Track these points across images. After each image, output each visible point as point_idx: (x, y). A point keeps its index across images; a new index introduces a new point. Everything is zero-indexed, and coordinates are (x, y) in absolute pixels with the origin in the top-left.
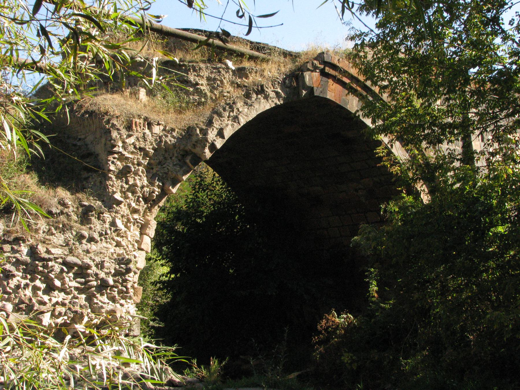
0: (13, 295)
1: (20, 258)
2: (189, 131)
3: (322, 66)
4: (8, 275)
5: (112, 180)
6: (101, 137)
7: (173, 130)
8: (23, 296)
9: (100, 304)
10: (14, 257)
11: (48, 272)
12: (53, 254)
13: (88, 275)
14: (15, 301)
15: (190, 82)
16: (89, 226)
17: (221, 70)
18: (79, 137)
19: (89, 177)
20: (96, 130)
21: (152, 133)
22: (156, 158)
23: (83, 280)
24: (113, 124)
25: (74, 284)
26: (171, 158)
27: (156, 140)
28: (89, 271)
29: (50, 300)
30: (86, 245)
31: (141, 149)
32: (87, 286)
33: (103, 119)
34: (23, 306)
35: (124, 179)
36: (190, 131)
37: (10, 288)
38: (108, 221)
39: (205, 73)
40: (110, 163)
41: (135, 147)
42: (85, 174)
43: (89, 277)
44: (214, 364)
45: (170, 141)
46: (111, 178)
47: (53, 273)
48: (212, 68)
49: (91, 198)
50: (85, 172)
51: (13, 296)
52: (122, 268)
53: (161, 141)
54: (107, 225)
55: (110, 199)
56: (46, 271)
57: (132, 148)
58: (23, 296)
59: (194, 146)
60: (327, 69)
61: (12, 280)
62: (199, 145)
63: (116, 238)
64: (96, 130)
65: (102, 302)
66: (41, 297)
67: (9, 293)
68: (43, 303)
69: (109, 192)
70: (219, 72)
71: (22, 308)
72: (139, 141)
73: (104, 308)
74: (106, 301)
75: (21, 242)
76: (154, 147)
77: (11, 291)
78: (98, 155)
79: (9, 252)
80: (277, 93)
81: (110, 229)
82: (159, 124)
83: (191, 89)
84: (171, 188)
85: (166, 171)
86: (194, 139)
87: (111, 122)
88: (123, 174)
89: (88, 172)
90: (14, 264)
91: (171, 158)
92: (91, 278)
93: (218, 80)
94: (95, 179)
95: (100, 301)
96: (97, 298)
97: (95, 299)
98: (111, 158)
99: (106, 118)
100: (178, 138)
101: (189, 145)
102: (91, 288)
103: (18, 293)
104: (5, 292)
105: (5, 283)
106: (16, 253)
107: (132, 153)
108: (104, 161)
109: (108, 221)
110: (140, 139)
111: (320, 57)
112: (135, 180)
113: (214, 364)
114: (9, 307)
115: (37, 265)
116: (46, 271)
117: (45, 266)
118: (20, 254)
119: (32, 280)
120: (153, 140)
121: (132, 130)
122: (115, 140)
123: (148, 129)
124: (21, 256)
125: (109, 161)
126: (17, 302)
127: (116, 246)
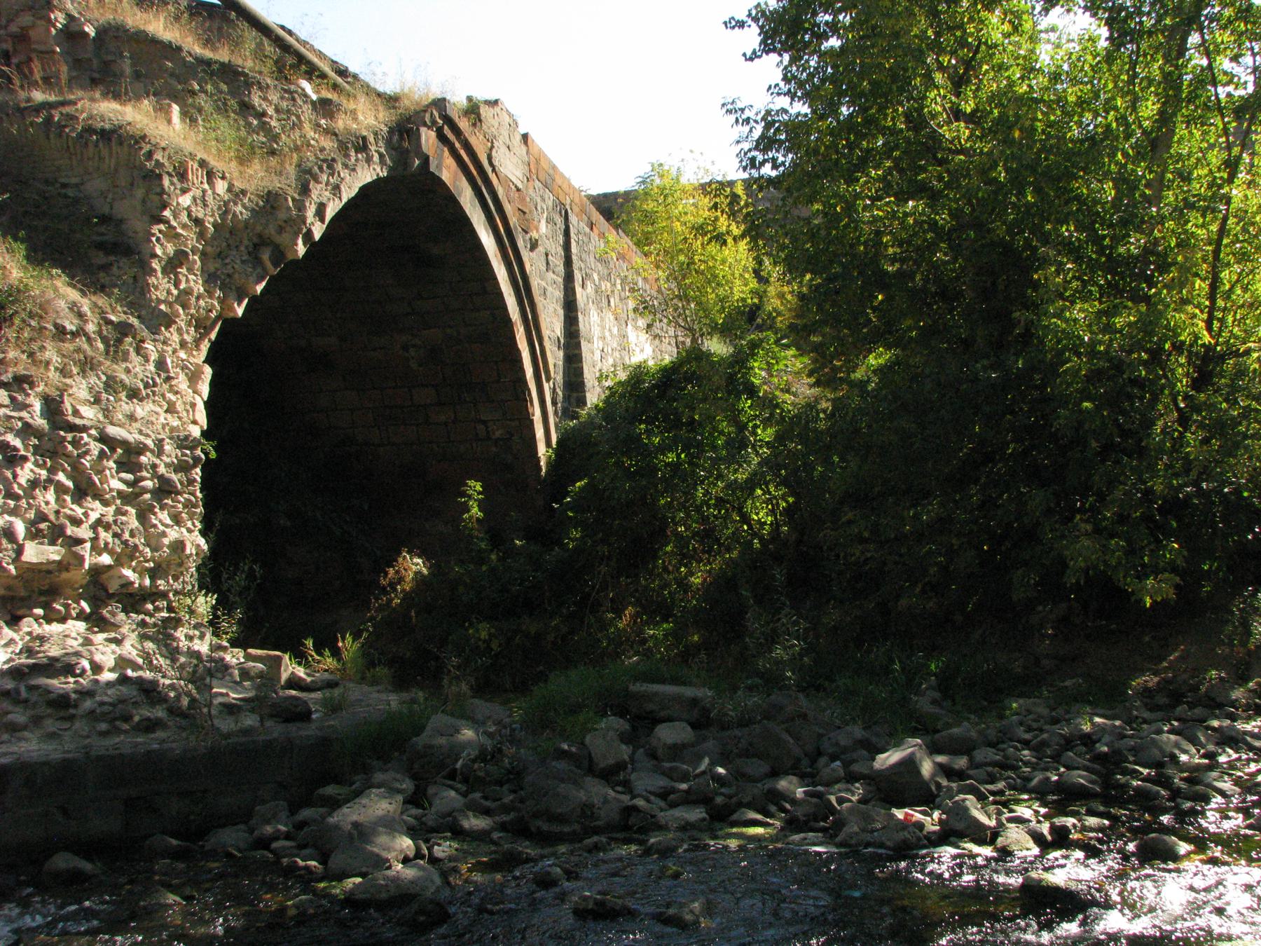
0: (24, 500)
1: (30, 421)
2: (272, 200)
3: (441, 122)
4: (14, 460)
5: (156, 276)
6: (132, 184)
7: (244, 192)
8: (43, 504)
9: (161, 528)
10: (20, 419)
11: (79, 456)
12: (82, 418)
13: (140, 467)
14: (28, 516)
15: (253, 107)
16: (124, 366)
17: (296, 96)
18: (63, 180)
19: (111, 264)
20: (116, 170)
21: (214, 193)
22: (216, 243)
23: (130, 477)
24: (157, 161)
25: (116, 484)
26: (237, 247)
27: (219, 208)
28: (143, 459)
29: (86, 514)
30: (127, 403)
31: (198, 222)
32: (137, 490)
33: (141, 148)
34: (43, 526)
35: (172, 276)
36: (271, 199)
37: (20, 485)
38: (153, 358)
39: (274, 97)
40: (154, 239)
41: (189, 216)
42: (100, 258)
43: (140, 471)
44: (348, 645)
45: (241, 213)
46: (155, 271)
47: (88, 458)
48: (283, 89)
49: (119, 308)
50: (101, 254)
51: (23, 503)
52: (186, 455)
53: (226, 212)
54: (151, 367)
55: (152, 313)
56: (75, 452)
57: (184, 218)
58: (43, 504)
59: (281, 230)
60: (447, 130)
61: (22, 468)
62: (288, 229)
63: (170, 396)
64: (116, 170)
65: (163, 524)
66: (71, 509)
67: (17, 498)
68: (77, 522)
69: (151, 300)
70: (294, 99)
71: (42, 530)
72: (196, 205)
73: (166, 536)
74: (168, 521)
75: (26, 386)
76: (215, 220)
77: (21, 492)
78: (121, 221)
79: (6, 406)
80: (381, 156)
81: (159, 376)
82: (223, 178)
83: (255, 122)
84: (236, 305)
85: (231, 271)
86: (282, 215)
87: (155, 157)
88: (174, 264)
89: (107, 254)
90: (18, 434)
91: (237, 247)
92: (145, 474)
93: (293, 114)
94: (124, 270)
95: (161, 521)
96: (155, 514)
97: (153, 517)
98: (155, 229)
99: (146, 148)
100: (253, 210)
101: (271, 226)
102: (142, 494)
103: (34, 498)
104: (10, 495)
105: (9, 474)
106: (20, 410)
107: (184, 226)
108: (141, 235)
109: (153, 358)
110: (198, 201)
111: (440, 103)
112: (188, 281)
113: (348, 645)
114: (20, 528)
115: (64, 439)
116: (75, 452)
117: (76, 443)
118: (29, 413)
119: (52, 471)
120: (215, 208)
121: (188, 180)
122: (169, 195)
123: (208, 183)
124: (32, 417)
125: (154, 235)
126: (33, 516)
127: (166, 412)
